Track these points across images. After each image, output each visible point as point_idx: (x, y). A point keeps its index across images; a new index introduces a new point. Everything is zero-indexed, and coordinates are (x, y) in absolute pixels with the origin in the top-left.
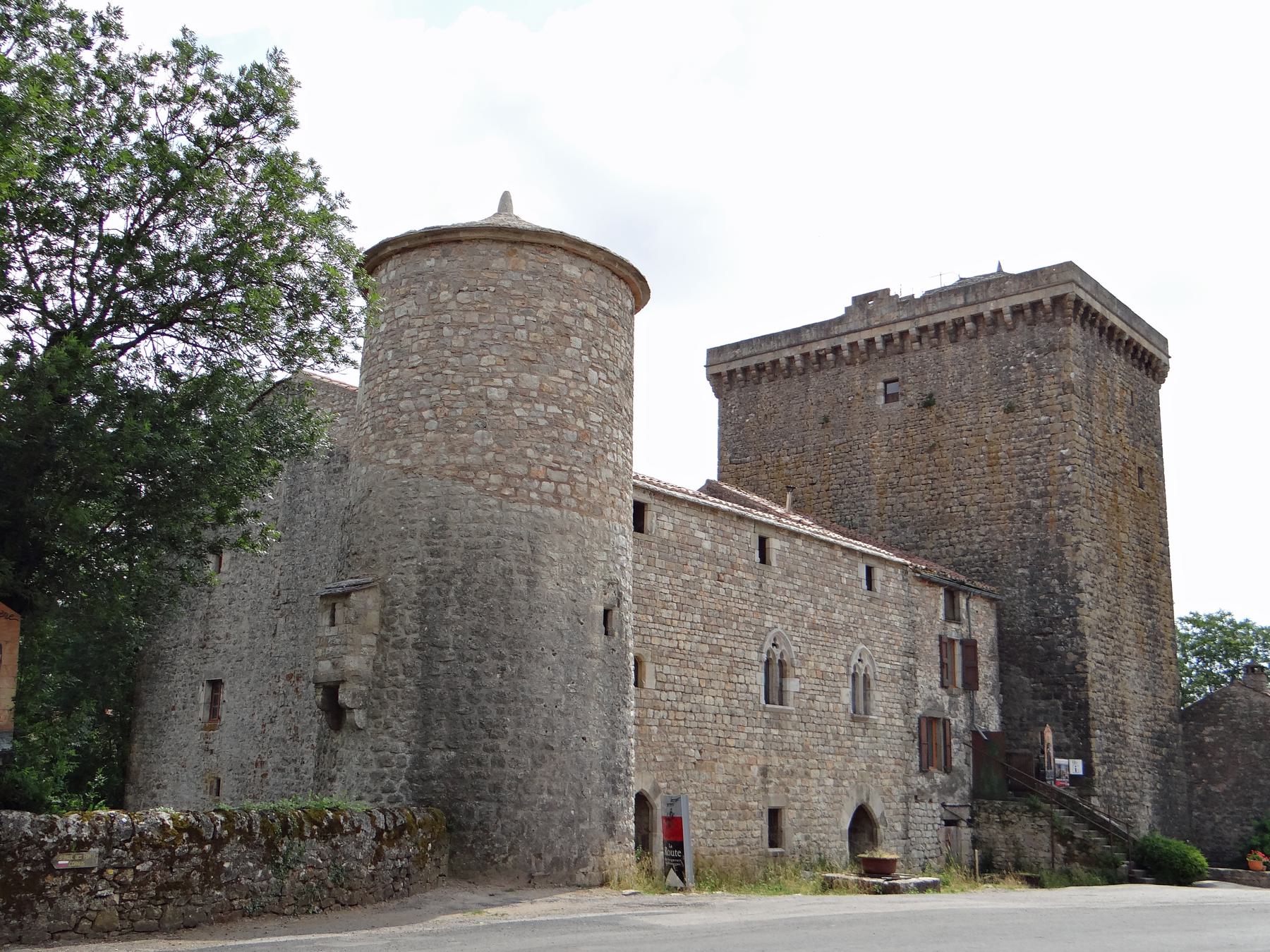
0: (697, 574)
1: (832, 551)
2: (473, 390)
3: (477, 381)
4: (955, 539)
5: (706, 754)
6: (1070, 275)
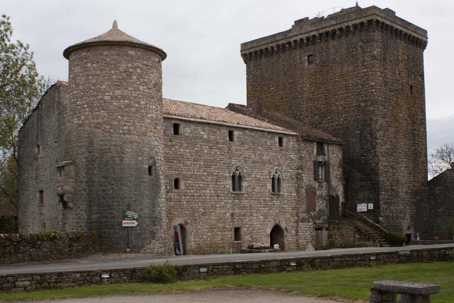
0: (201, 147)
1: (263, 133)
2: (99, 97)
3: (100, 94)
4: (334, 120)
5: (207, 210)
6: (373, 12)
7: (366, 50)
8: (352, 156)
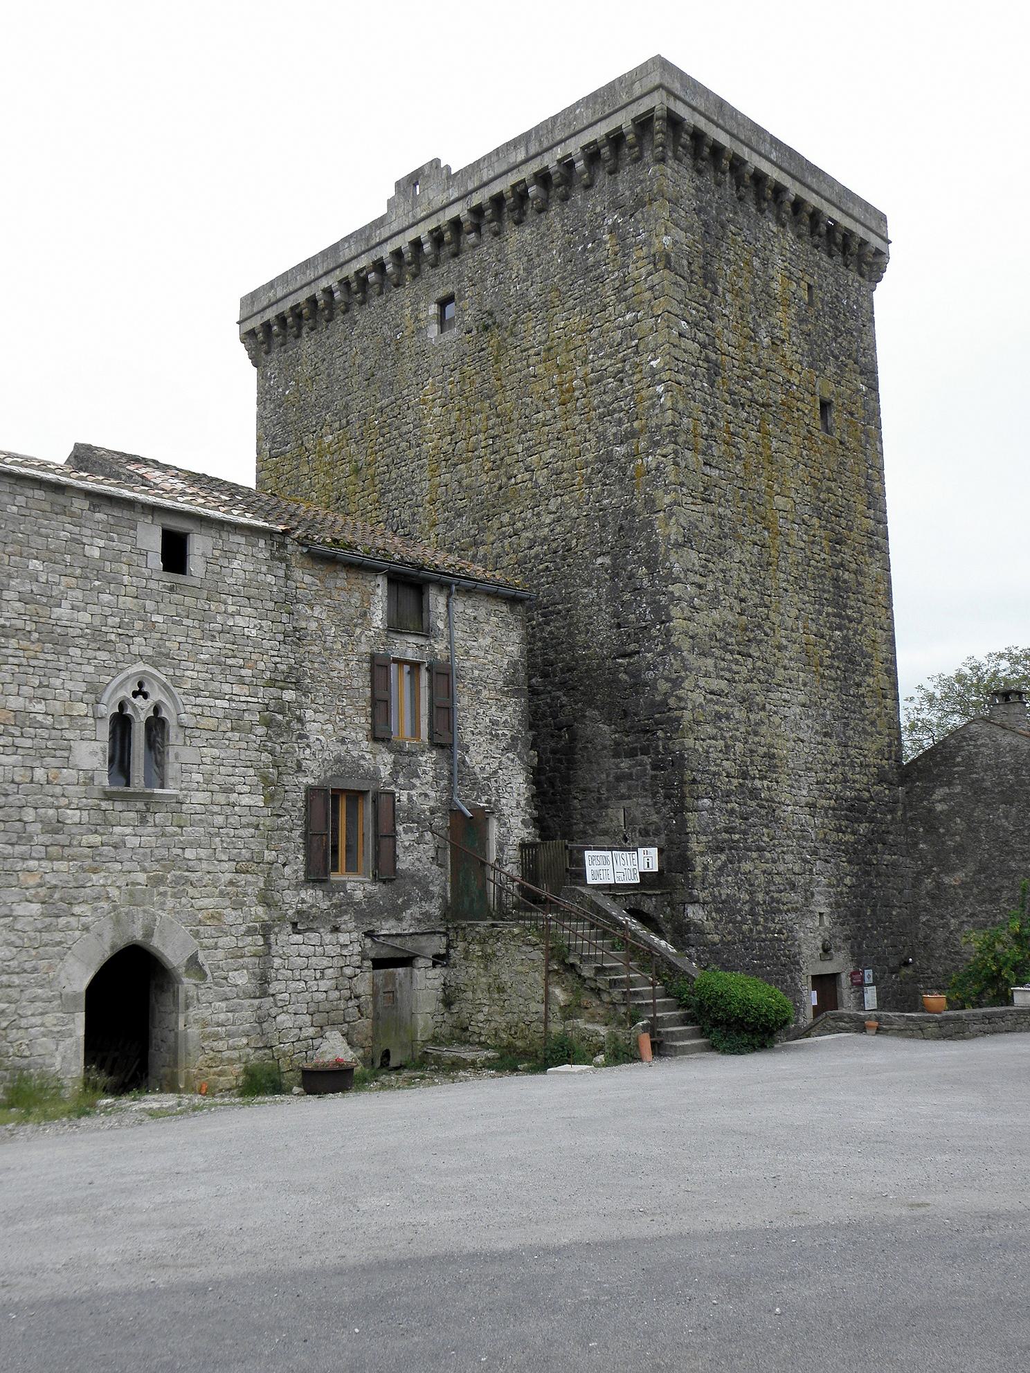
1: (61, 499)
4: (519, 524)
7: (631, 240)
8: (584, 657)
